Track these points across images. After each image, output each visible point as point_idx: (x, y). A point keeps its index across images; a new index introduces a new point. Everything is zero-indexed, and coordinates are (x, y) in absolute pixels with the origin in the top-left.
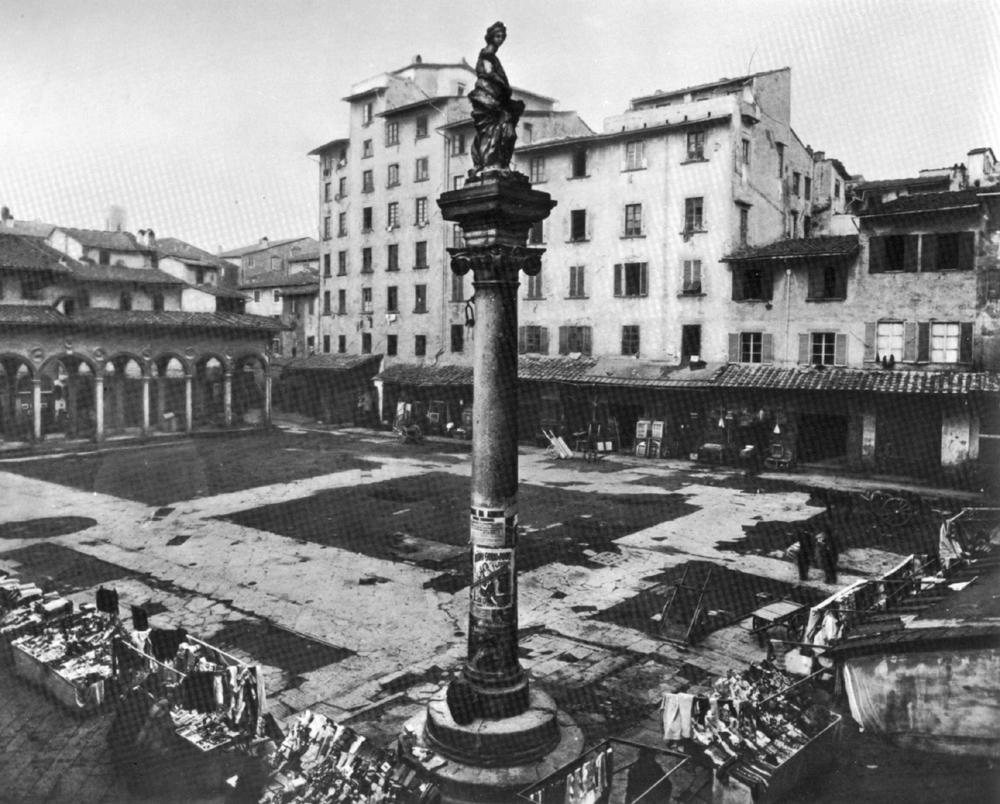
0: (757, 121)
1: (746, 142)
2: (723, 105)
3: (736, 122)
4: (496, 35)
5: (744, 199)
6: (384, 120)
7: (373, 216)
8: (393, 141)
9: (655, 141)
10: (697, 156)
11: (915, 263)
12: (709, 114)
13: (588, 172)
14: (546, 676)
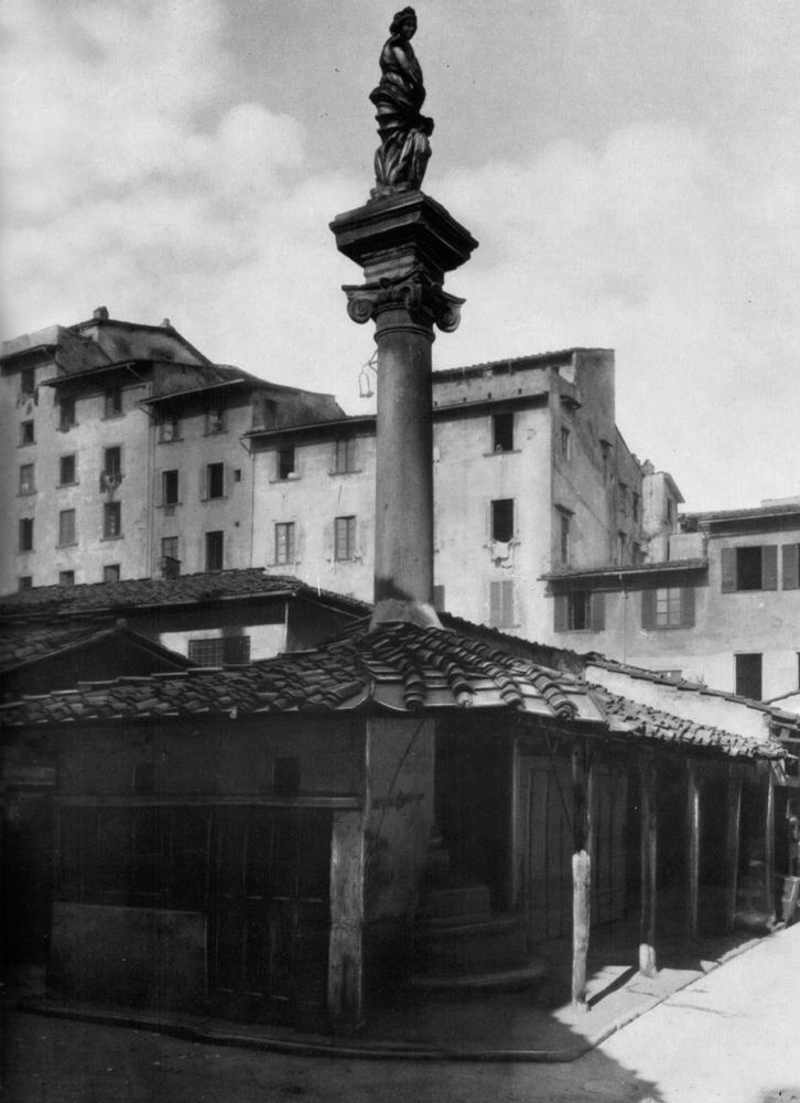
0: (579, 406)
1: (565, 431)
2: (535, 382)
3: (555, 400)
4: (404, 24)
5: (566, 504)
6: (52, 391)
7: (724, 515)
8: (68, 420)
9: (449, 425)
10: (504, 440)
11: (775, 581)
12: (465, 399)
13: (517, 444)
14: (134, 604)
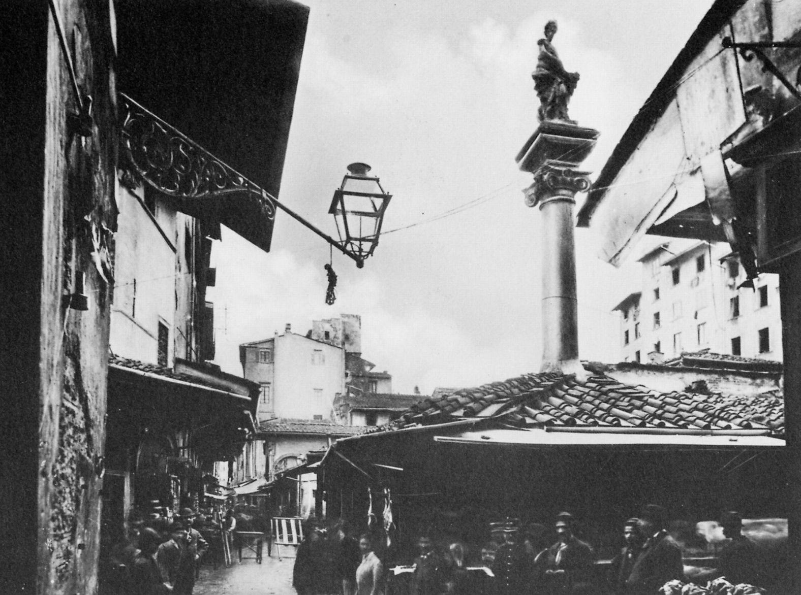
4: (550, 29)
